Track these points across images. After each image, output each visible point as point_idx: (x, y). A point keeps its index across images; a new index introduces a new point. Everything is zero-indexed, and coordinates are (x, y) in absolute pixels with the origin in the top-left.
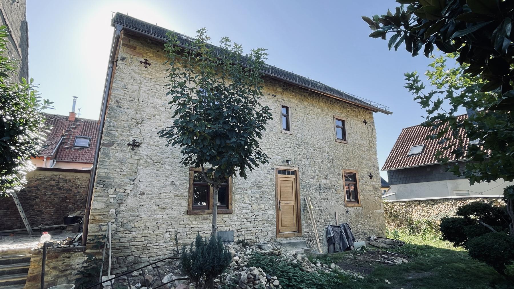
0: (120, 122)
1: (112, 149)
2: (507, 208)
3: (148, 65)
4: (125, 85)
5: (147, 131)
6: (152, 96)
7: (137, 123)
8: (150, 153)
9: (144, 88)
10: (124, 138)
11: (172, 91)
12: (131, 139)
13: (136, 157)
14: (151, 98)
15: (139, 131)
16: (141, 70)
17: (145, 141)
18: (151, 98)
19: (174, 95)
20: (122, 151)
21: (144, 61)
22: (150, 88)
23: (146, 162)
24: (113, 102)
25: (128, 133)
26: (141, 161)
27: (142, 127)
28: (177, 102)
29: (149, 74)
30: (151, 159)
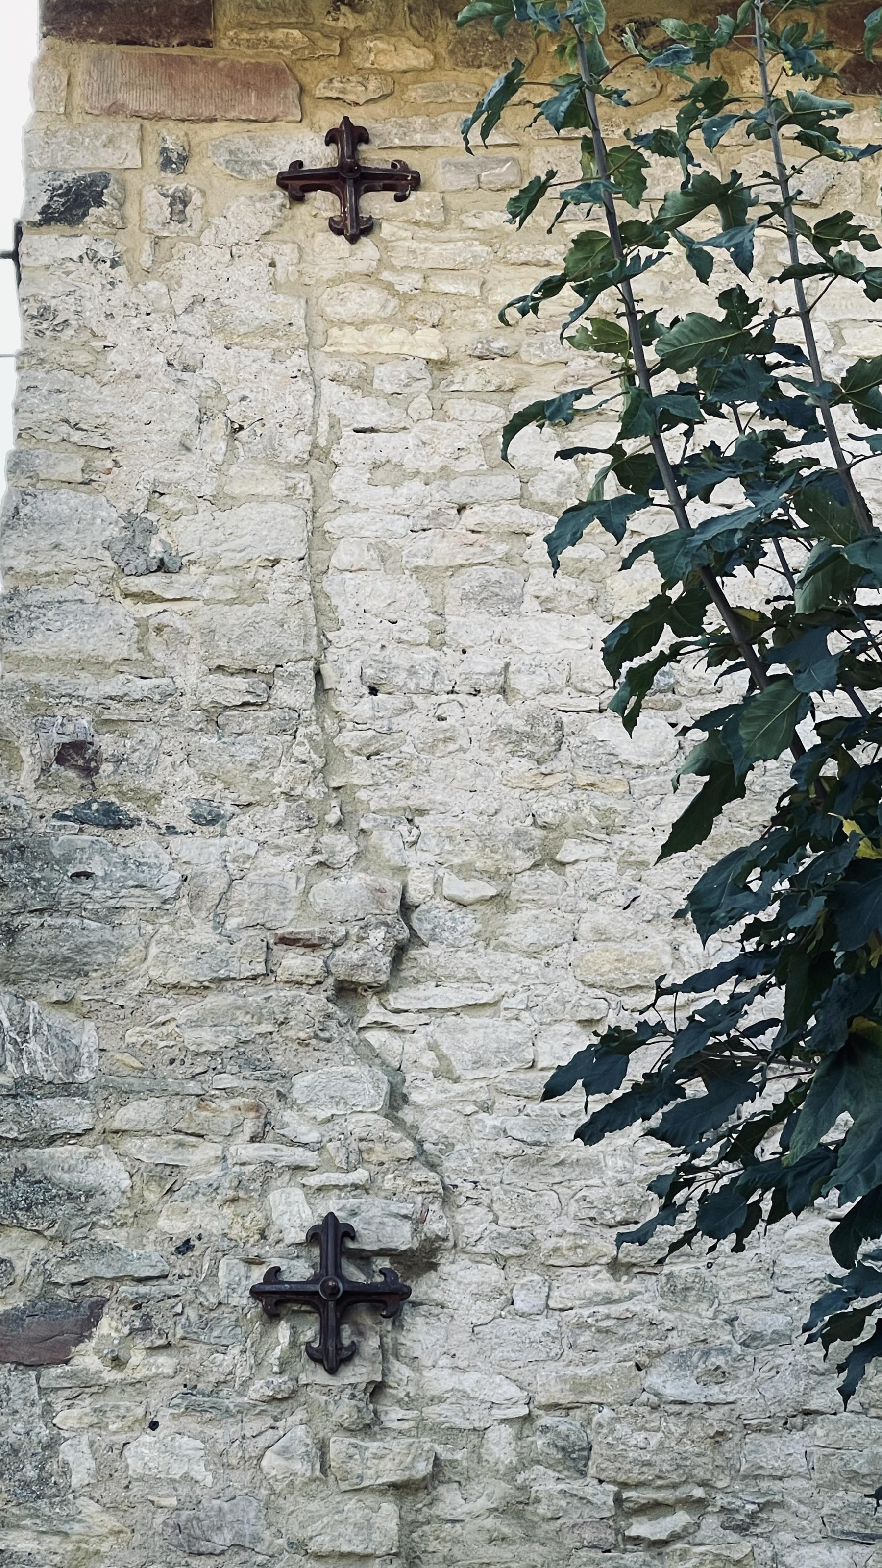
0: (132, 1013)
1: (87, 1386)
2: (655, 1120)
3: (377, 204)
4: (136, 528)
5: (472, 1084)
6: (487, 597)
7: (346, 991)
8: (550, 1385)
9: (366, 512)
10: (208, 1219)
11: (625, 467)
12: (294, 1213)
13: (390, 1458)
14: (470, 625)
15: (370, 1091)
16: (301, 288)
17: (473, 1221)
18: (470, 625)
19: (652, 521)
20: (200, 1399)
21: (320, 155)
22: (438, 496)
23: (517, 1507)
24: (26, 777)
25: (244, 1150)
26: (451, 1500)
27: (412, 1029)
28: (713, 619)
29: (405, 310)
30: (575, 1457)
